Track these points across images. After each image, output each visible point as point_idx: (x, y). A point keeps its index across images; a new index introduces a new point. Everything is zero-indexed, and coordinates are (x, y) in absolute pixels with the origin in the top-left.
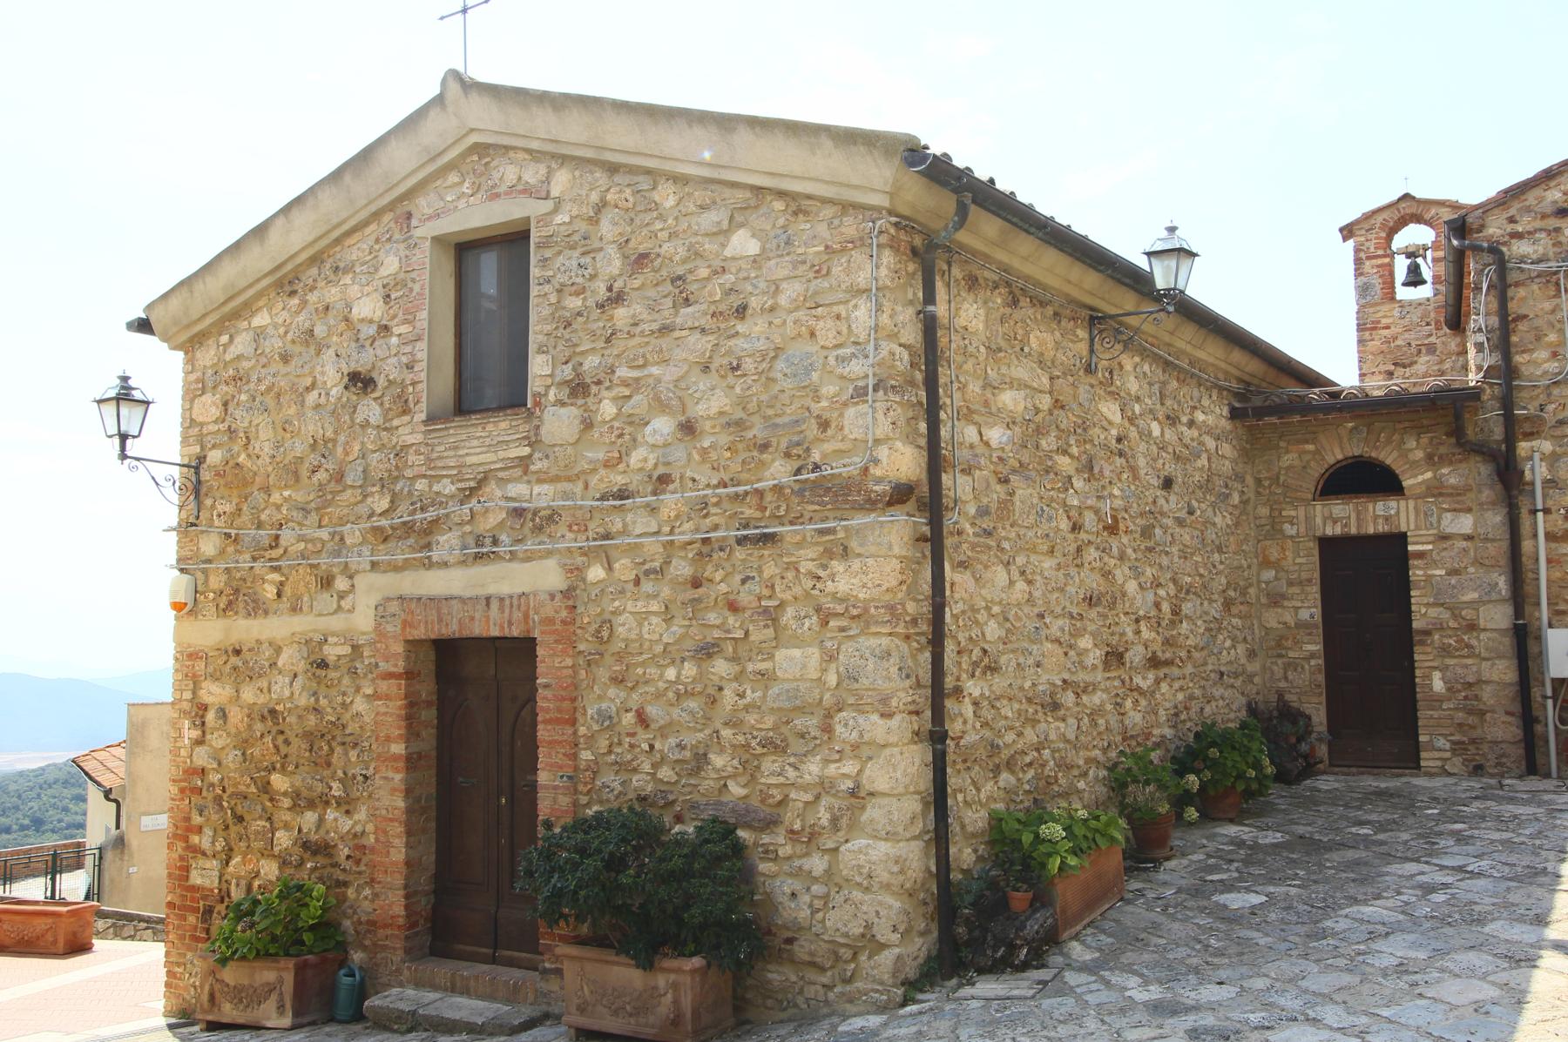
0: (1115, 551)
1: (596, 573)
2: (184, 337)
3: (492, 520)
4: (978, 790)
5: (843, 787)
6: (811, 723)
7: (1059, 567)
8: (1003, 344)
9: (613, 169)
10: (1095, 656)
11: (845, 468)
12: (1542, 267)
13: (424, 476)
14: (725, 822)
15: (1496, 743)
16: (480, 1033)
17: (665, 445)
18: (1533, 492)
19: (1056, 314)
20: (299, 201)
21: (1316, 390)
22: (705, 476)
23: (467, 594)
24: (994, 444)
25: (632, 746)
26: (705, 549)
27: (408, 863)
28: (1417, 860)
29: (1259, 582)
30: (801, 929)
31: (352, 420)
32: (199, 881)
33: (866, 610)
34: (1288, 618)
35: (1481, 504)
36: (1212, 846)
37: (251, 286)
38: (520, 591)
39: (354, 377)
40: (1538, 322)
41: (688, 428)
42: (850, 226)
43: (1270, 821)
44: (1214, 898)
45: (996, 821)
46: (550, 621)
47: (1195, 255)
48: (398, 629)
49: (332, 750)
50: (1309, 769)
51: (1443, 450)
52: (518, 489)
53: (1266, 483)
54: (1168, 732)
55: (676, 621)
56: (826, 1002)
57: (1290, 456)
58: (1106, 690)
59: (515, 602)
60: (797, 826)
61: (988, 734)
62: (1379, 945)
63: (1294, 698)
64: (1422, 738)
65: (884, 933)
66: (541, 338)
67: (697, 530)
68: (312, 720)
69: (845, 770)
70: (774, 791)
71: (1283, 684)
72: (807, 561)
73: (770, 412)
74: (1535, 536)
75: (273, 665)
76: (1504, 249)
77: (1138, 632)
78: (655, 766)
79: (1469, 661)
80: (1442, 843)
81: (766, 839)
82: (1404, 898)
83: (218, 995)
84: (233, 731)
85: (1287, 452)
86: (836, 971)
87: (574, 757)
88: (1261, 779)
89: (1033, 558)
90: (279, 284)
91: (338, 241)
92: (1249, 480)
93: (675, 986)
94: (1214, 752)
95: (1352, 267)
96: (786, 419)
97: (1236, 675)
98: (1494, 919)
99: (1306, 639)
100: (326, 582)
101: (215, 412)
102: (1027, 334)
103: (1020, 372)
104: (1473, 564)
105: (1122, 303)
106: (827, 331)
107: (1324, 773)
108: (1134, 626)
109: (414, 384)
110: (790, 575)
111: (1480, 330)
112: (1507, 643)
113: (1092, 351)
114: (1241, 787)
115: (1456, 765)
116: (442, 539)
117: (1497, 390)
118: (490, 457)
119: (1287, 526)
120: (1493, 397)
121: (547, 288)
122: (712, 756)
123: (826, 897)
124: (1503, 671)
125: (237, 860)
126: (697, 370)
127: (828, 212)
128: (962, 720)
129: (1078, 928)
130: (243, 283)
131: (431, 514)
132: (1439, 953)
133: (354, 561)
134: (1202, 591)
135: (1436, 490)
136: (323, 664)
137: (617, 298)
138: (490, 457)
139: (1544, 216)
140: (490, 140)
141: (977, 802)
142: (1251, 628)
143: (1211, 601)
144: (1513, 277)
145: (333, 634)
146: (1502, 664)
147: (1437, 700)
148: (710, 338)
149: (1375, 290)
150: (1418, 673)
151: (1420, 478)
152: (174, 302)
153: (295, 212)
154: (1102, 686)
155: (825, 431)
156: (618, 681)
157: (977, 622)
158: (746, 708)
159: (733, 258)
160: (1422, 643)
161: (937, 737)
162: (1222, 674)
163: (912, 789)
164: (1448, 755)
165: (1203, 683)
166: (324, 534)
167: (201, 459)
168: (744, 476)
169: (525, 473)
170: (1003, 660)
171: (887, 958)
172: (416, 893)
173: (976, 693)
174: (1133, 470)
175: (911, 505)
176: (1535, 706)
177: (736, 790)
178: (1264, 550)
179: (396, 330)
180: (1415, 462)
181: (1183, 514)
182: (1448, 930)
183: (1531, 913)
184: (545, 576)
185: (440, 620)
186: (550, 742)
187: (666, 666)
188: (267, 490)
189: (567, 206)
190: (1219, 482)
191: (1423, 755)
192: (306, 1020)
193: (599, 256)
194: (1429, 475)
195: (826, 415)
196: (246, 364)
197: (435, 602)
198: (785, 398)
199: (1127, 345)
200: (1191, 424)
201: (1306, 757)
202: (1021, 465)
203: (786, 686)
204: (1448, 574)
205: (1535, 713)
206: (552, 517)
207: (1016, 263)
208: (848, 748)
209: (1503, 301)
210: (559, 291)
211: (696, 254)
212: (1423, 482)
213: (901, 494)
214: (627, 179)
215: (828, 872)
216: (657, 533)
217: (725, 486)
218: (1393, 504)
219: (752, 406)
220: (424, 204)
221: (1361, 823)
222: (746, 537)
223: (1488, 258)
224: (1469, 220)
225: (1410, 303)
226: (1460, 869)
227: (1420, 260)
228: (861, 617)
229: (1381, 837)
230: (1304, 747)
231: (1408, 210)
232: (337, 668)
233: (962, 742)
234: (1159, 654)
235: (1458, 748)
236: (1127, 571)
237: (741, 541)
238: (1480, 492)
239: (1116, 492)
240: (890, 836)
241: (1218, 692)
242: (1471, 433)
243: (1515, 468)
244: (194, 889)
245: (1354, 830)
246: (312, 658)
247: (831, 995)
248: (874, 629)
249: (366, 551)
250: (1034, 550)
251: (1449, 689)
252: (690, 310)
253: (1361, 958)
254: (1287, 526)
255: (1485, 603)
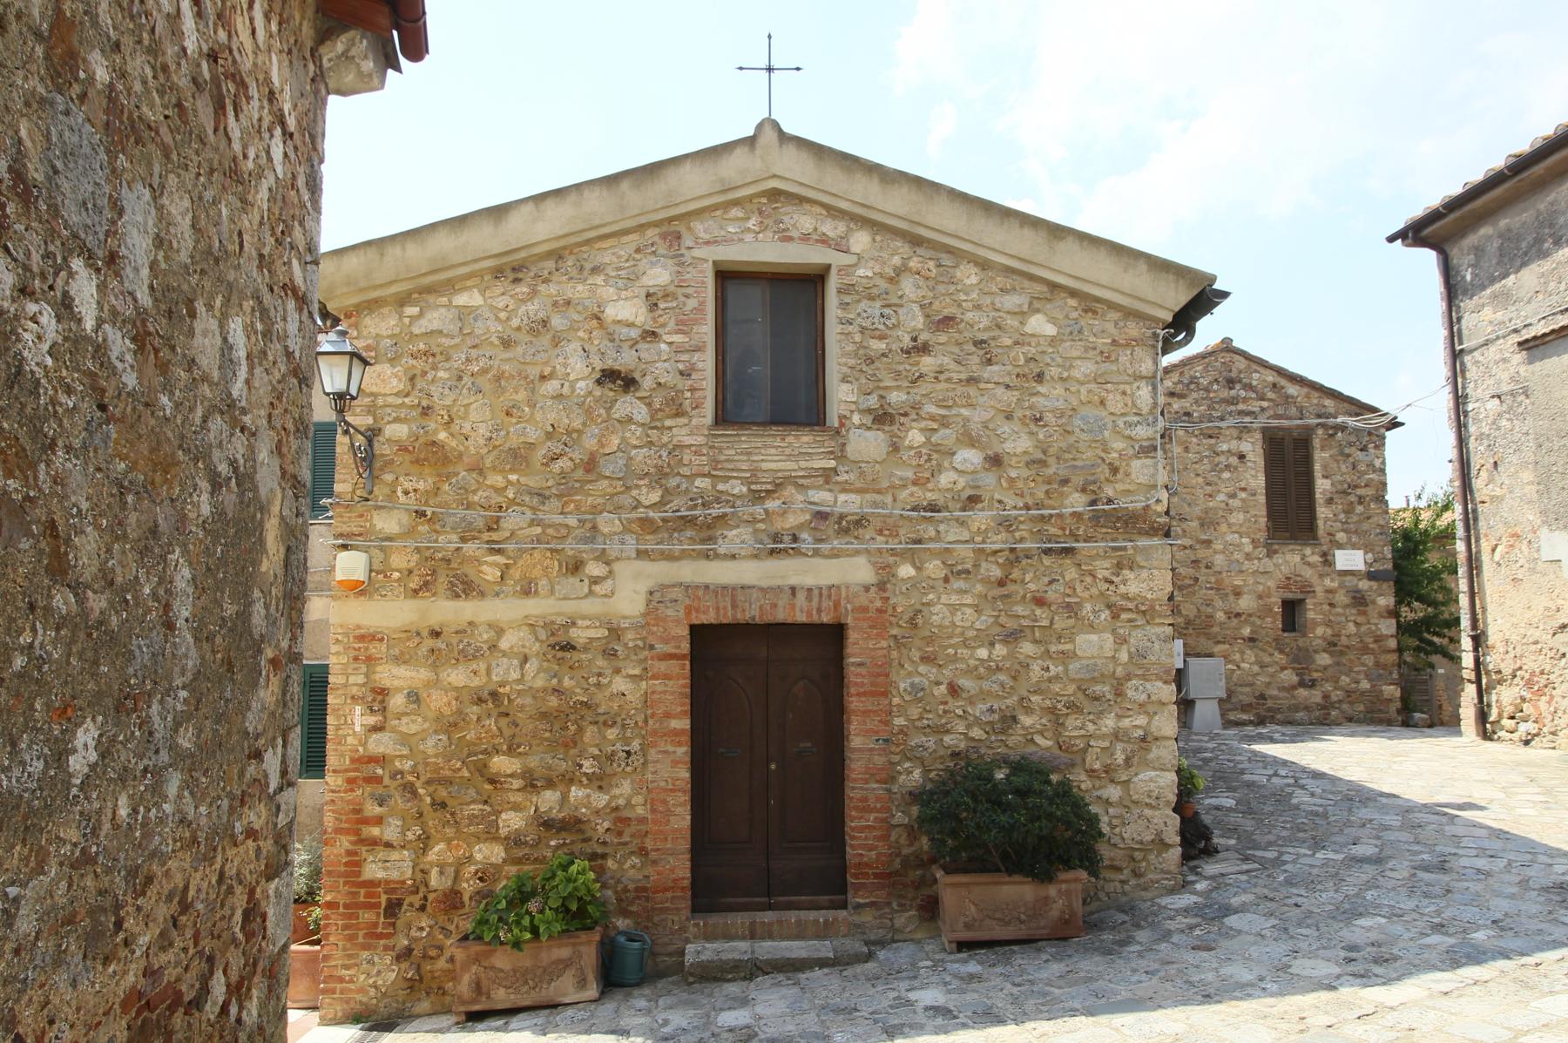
1: (906, 571)
3: (792, 521)
9: (916, 241)
13: (708, 475)
17: (973, 472)
32: (380, 875)
37: (464, 264)
38: (830, 583)
39: (609, 376)
41: (995, 461)
42: (1134, 329)
48: (682, 614)
52: (821, 496)
56: (1124, 893)
59: (825, 592)
68: (553, 702)
69: (1137, 723)
72: (1103, 568)
75: (493, 647)
78: (969, 727)
83: (484, 983)
84: (431, 715)
87: (887, 723)
90: (498, 273)
91: (588, 242)
100: (576, 567)
106: (1115, 403)
116: (732, 533)
118: (790, 465)
131: (715, 511)
133: (613, 549)
136: (569, 647)
138: (790, 465)
145: (584, 618)
153: (549, 204)
156: (926, 659)
158: (1049, 680)
169: (827, 482)
184: (854, 571)
185: (734, 606)
193: (900, 311)
195: (1117, 463)
197: (732, 592)
203: (1085, 662)
206: (860, 522)
214: (929, 253)
222: (1050, 549)
228: (1147, 613)
232: (586, 649)
246: (552, 640)
247: (1127, 888)
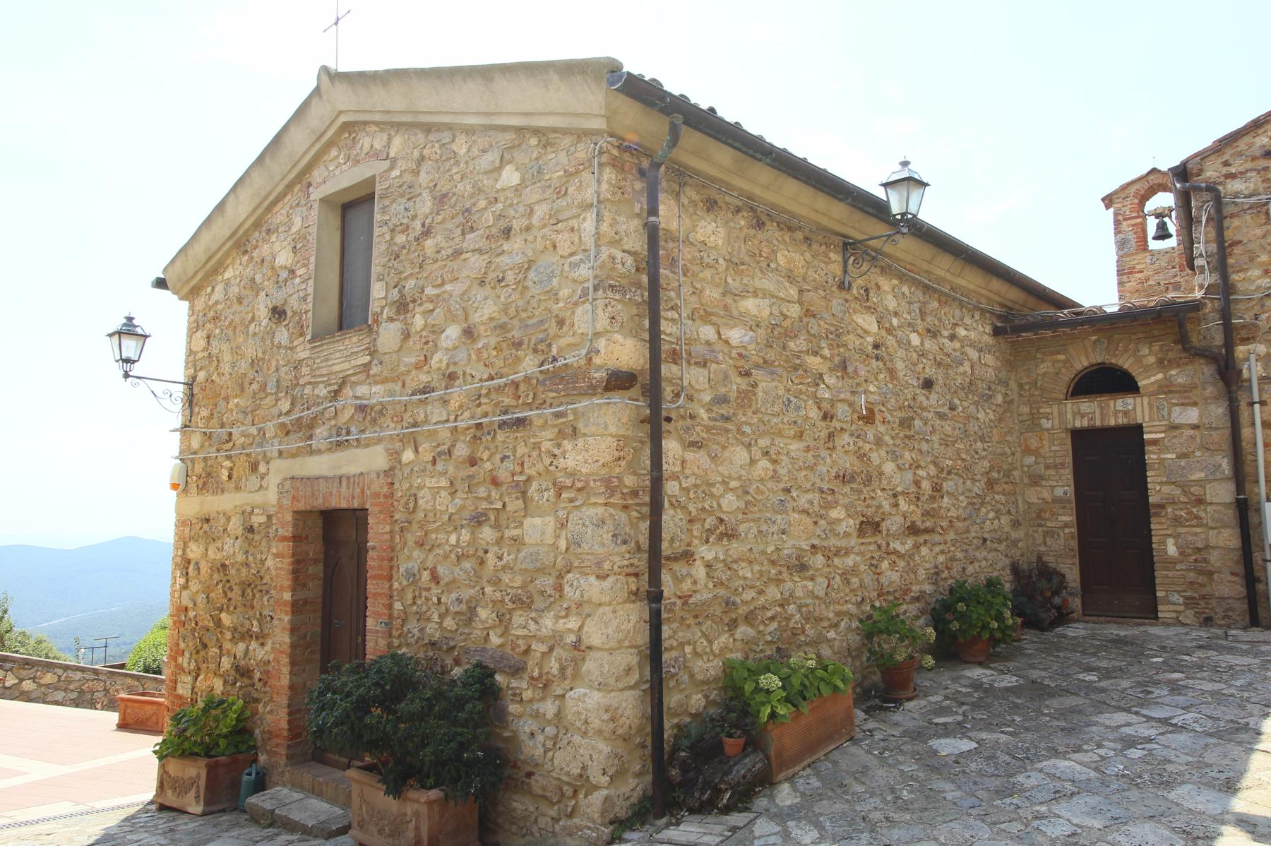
0: (870, 437)
2: (185, 290)
4: (710, 642)
5: (568, 641)
6: (545, 582)
7: (808, 449)
8: (747, 259)
9: (428, 128)
10: (850, 525)
11: (574, 359)
12: (1253, 200)
13: (310, 383)
14: (486, 667)
15: (1222, 598)
16: (309, 834)
17: (455, 348)
18: (1250, 388)
19: (806, 238)
20: (241, 181)
21: (1066, 311)
22: (480, 372)
23: (331, 474)
24: (734, 342)
25: (427, 599)
26: (478, 434)
27: (291, 687)
28: (1128, 710)
29: (1022, 466)
30: (537, 765)
31: (272, 343)
33: (587, 483)
34: (1046, 494)
35: (1205, 399)
36: (954, 687)
37: (219, 249)
40: (1250, 247)
41: (469, 333)
42: (583, 151)
43: (1011, 665)
44: (930, 743)
45: (729, 668)
46: (376, 495)
47: (926, 185)
49: (254, 595)
50: (1063, 617)
51: (1171, 355)
52: (362, 390)
53: (1027, 387)
54: (928, 588)
55: (458, 494)
57: (1045, 365)
58: (860, 553)
60: (536, 674)
61: (721, 592)
62: (1061, 808)
63: (1052, 559)
64: (1159, 594)
65: (596, 777)
66: (379, 269)
67: (472, 417)
69: (570, 626)
70: (520, 642)
71: (1043, 548)
72: (546, 438)
73: (524, 315)
74: (1253, 424)
76: (1220, 188)
77: (896, 505)
78: (442, 616)
79: (1198, 530)
80: (1157, 692)
81: (514, 684)
82: (1102, 752)
85: (1043, 362)
86: (562, 806)
87: (390, 606)
88: (1004, 629)
89: (778, 440)
92: (1013, 385)
93: (417, 814)
94: (961, 606)
95: (1113, 227)
96: (534, 321)
97: (1000, 541)
98: (1183, 782)
99: (1061, 511)
100: (254, 467)
101: (203, 343)
102: (774, 252)
103: (766, 283)
104: (1199, 449)
105: (868, 231)
107: (1077, 621)
108: (892, 500)
109: (306, 312)
110: (535, 454)
111: (1201, 255)
112: (1230, 515)
113: (845, 272)
114: (986, 636)
115: (1189, 616)
116: (318, 431)
117: (1217, 304)
118: (346, 366)
119: (1044, 421)
120: (1214, 310)
121: (385, 229)
122: (479, 609)
123: (555, 739)
124: (1228, 538)
125: (202, 677)
126: (476, 286)
127: (567, 141)
128: (687, 582)
129: (797, 769)
130: (215, 247)
132: (1117, 822)
134: (967, 472)
135: (1166, 388)
136: (251, 530)
137: (427, 232)
138: (346, 366)
139: (1254, 159)
140: (351, 119)
141: (701, 657)
142: (1016, 503)
143: (973, 480)
144: (1228, 210)
146: (1226, 533)
147: (1172, 562)
148: (485, 257)
149: (1131, 243)
150: (1154, 539)
151: (1153, 379)
152: (178, 264)
154: (856, 550)
155: (561, 328)
156: (420, 544)
157: (712, 495)
158: (504, 568)
159: (503, 190)
160: (1157, 515)
161: (655, 596)
162: (985, 540)
163: (627, 643)
164: (1181, 608)
165: (965, 547)
166: (253, 430)
167: (194, 378)
168: (505, 370)
169: (368, 376)
170: (742, 528)
171: (597, 798)
172: (299, 711)
173: (710, 556)
174: (892, 372)
175: (635, 391)
176: (1256, 568)
177: (495, 640)
178: (1026, 440)
179: (298, 273)
180: (1148, 366)
181: (945, 410)
182: (1134, 794)
183: (1223, 776)
186: (375, 595)
187: (451, 532)
188: (227, 399)
189: (399, 163)
190: (981, 386)
191: (1160, 608)
192: (219, 807)
193: (418, 200)
194: (1160, 376)
195: (562, 315)
196: (220, 307)
197: (311, 480)
198: (534, 303)
199: (884, 270)
200: (952, 337)
201: (1059, 609)
202: (765, 362)
204: (1178, 457)
205: (1257, 574)
207: (757, 191)
208: (574, 606)
209: (1220, 231)
210: (393, 231)
211: (479, 190)
212: (1156, 382)
213: (619, 381)
215: (558, 714)
216: (447, 421)
217: (492, 379)
218: (1130, 400)
219: (512, 311)
220: (317, 175)
221: (1090, 669)
223: (1206, 196)
224: (1189, 166)
225: (1159, 252)
226: (1165, 721)
227: (1166, 219)
229: (1103, 684)
230: (1057, 600)
231: (1152, 183)
232: (259, 532)
233: (690, 601)
234: (919, 523)
235: (1190, 602)
236: (884, 454)
237: (502, 425)
238: (1204, 389)
239: (872, 388)
240: (601, 687)
241: (980, 554)
242: (1195, 340)
243: (1234, 368)
244: (180, 697)
245: (1081, 676)
248: (593, 500)
249: (276, 441)
250: (780, 434)
251: (1181, 553)
252: (472, 235)
253: (1035, 824)
254: (1044, 421)
255: (1210, 481)
